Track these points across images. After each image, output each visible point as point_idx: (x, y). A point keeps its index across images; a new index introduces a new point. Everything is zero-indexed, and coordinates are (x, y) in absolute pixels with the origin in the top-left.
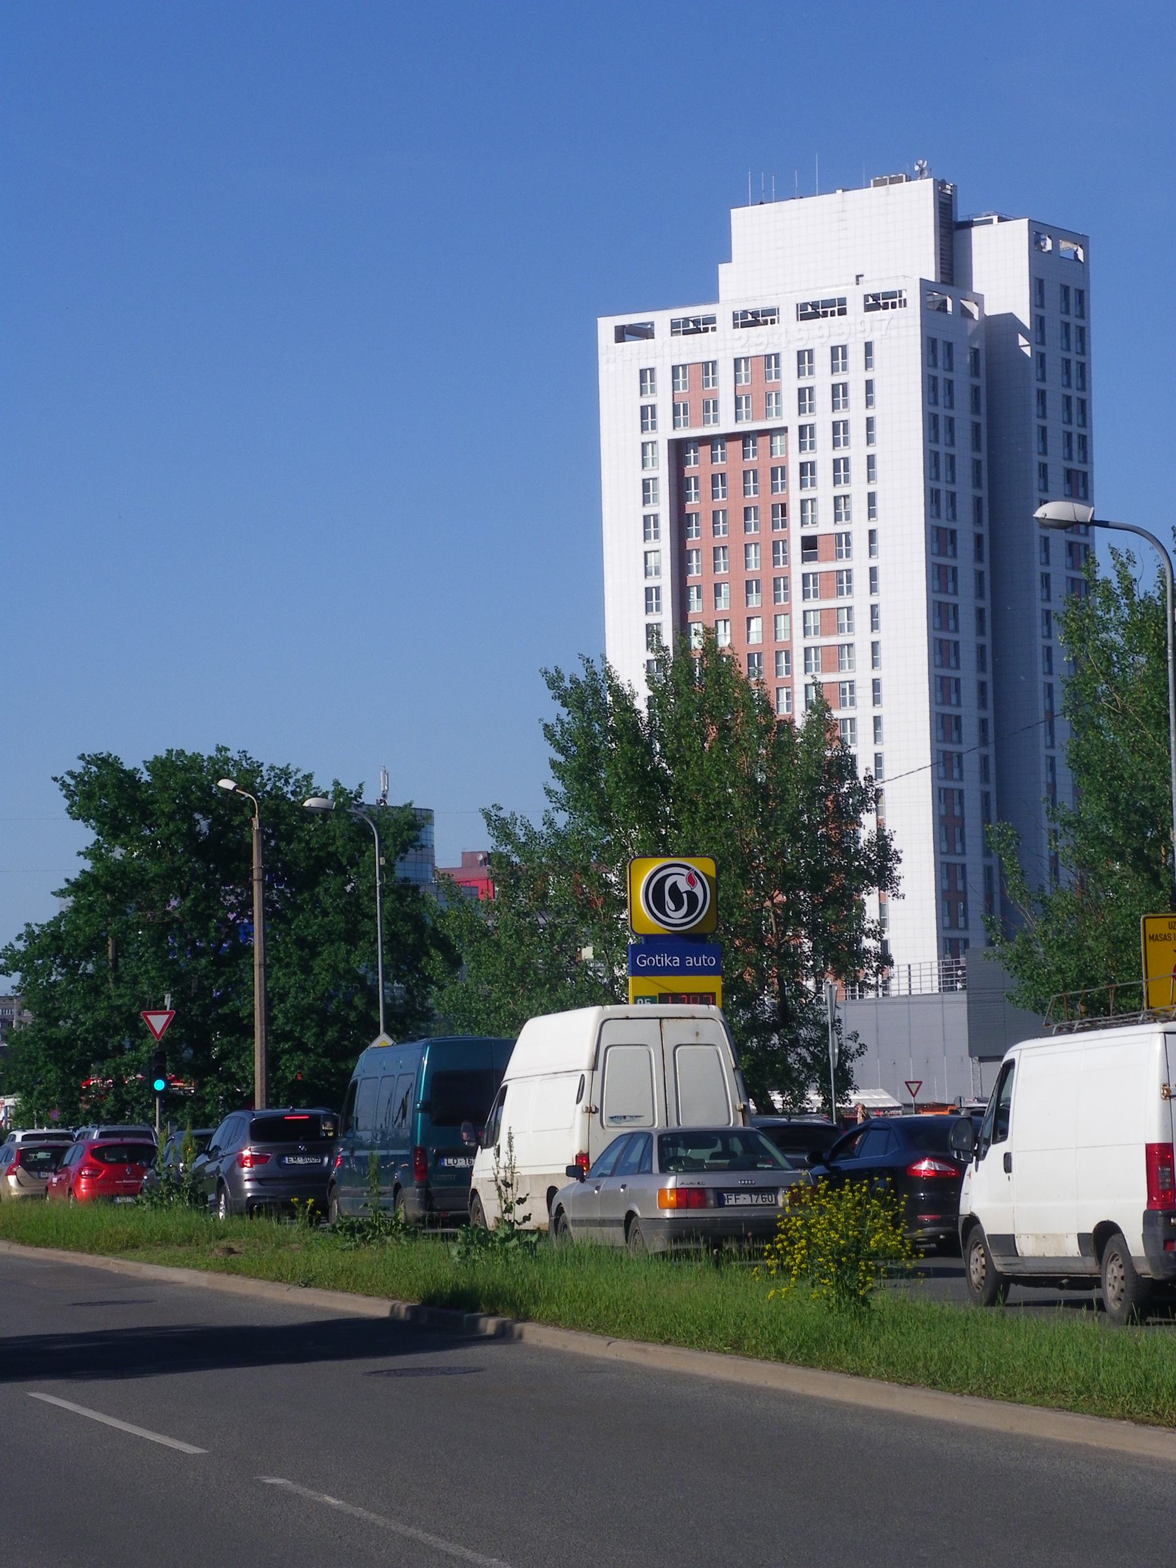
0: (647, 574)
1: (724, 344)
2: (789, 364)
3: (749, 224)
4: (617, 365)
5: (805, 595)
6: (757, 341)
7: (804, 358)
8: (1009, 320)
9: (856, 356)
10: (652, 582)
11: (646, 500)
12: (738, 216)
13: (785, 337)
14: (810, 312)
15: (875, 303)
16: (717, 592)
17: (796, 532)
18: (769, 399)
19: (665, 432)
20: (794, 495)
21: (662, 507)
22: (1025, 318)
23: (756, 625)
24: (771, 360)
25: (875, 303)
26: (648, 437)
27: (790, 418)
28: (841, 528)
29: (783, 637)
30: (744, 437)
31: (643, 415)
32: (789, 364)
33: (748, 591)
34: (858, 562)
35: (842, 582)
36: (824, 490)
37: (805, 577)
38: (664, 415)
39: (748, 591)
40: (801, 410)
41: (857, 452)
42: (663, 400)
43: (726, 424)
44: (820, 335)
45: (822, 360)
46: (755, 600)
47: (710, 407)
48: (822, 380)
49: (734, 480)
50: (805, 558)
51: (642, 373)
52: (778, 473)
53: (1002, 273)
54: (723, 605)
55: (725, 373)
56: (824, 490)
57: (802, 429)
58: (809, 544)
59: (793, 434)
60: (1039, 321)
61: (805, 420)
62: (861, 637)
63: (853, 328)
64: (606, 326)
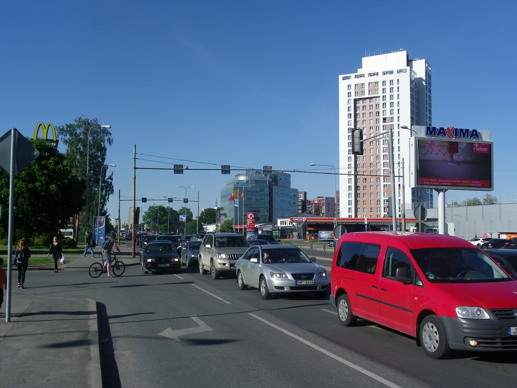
1: (366, 80)
2: (380, 84)
3: (366, 60)
4: (343, 85)
6: (374, 79)
7: (384, 82)
8: (421, 79)
9: (395, 82)
11: (349, 111)
12: (364, 59)
14: (384, 73)
15: (399, 71)
17: (381, 117)
18: (377, 90)
19: (353, 97)
20: (381, 109)
21: (352, 112)
22: (424, 78)
25: (399, 71)
26: (349, 98)
27: (381, 94)
28: (392, 116)
30: (370, 98)
32: (380, 84)
36: (388, 108)
38: (353, 94)
40: (383, 93)
41: (395, 101)
42: (353, 91)
43: (367, 95)
45: (388, 83)
46: (372, 131)
47: (363, 92)
48: (388, 86)
49: (368, 107)
50: (384, 122)
53: (420, 68)
55: (366, 86)
56: (388, 108)
58: (384, 119)
59: (381, 98)
60: (426, 79)
63: (395, 76)
64: (341, 77)
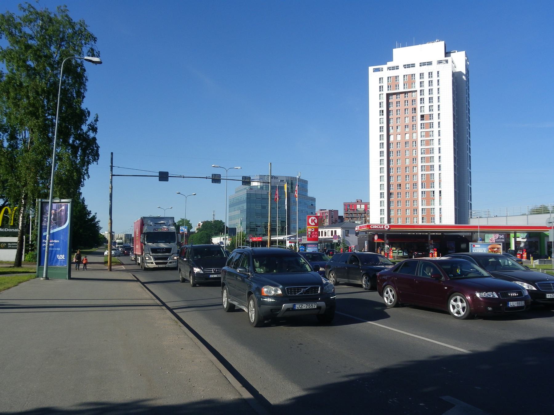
0: (380, 123)
4: (373, 77)
5: (422, 170)
6: (410, 71)
7: (422, 75)
10: (381, 125)
13: (417, 70)
16: (397, 128)
17: (419, 114)
19: (386, 91)
20: (419, 105)
21: (385, 149)
23: (407, 135)
24: (413, 75)
26: (381, 93)
27: (417, 87)
28: (431, 113)
29: (414, 138)
31: (381, 153)
33: (406, 127)
34: (435, 121)
35: (431, 125)
36: (427, 104)
37: (422, 166)
39: (406, 127)
41: (435, 96)
42: (385, 84)
43: (401, 89)
44: (426, 70)
45: (426, 75)
47: (397, 86)
48: (426, 79)
50: (421, 120)
51: (380, 79)
52: (414, 101)
54: (399, 130)
56: (427, 104)
57: (421, 90)
58: (422, 116)
59: (419, 92)
61: (422, 88)
62: (436, 155)
64: (371, 69)
